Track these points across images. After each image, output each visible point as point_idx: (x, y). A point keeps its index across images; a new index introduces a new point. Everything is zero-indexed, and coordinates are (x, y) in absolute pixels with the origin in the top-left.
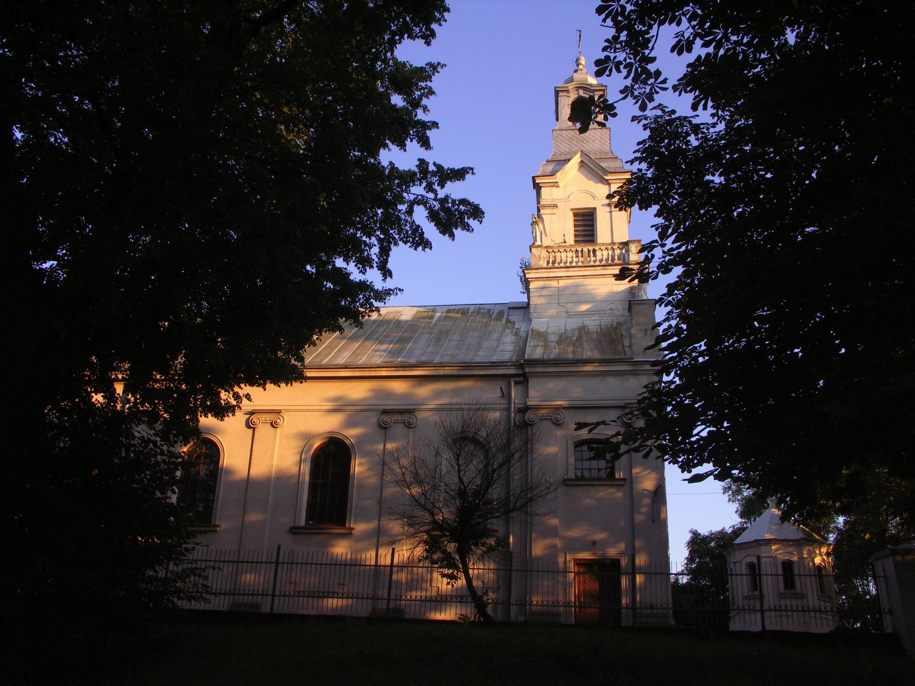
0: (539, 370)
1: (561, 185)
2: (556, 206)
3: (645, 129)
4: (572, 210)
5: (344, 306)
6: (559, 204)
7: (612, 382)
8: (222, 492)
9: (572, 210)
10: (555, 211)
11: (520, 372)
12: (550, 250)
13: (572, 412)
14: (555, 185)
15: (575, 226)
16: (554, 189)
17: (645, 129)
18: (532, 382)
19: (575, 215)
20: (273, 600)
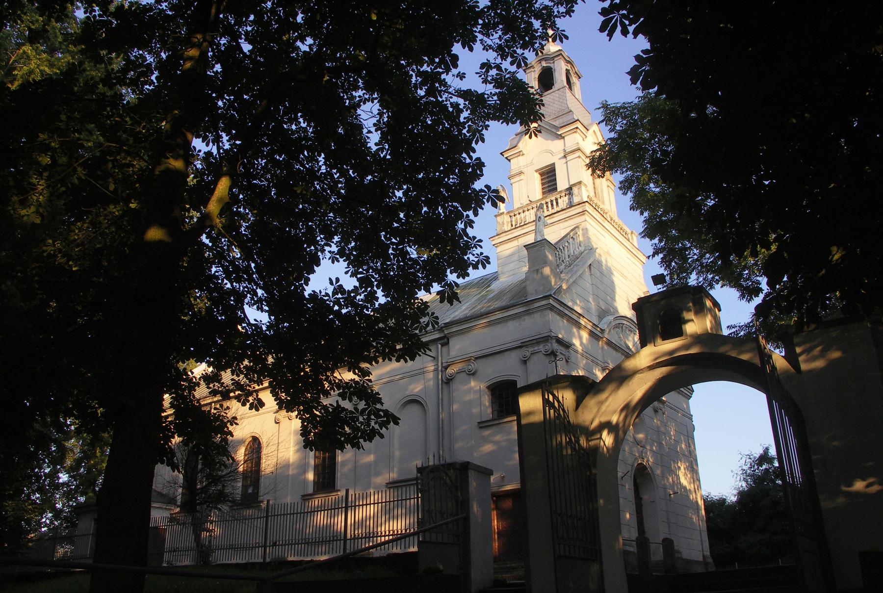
0: (455, 329)
1: (524, 152)
2: (521, 173)
3: (488, 126)
4: (536, 171)
5: (548, 276)
6: (523, 170)
7: (512, 325)
8: (262, 480)
9: (536, 171)
10: (522, 177)
11: (442, 335)
12: (512, 214)
13: (484, 360)
14: (520, 154)
15: (543, 184)
16: (521, 157)
17: (488, 126)
18: (452, 342)
19: (541, 175)
20: (265, 550)
